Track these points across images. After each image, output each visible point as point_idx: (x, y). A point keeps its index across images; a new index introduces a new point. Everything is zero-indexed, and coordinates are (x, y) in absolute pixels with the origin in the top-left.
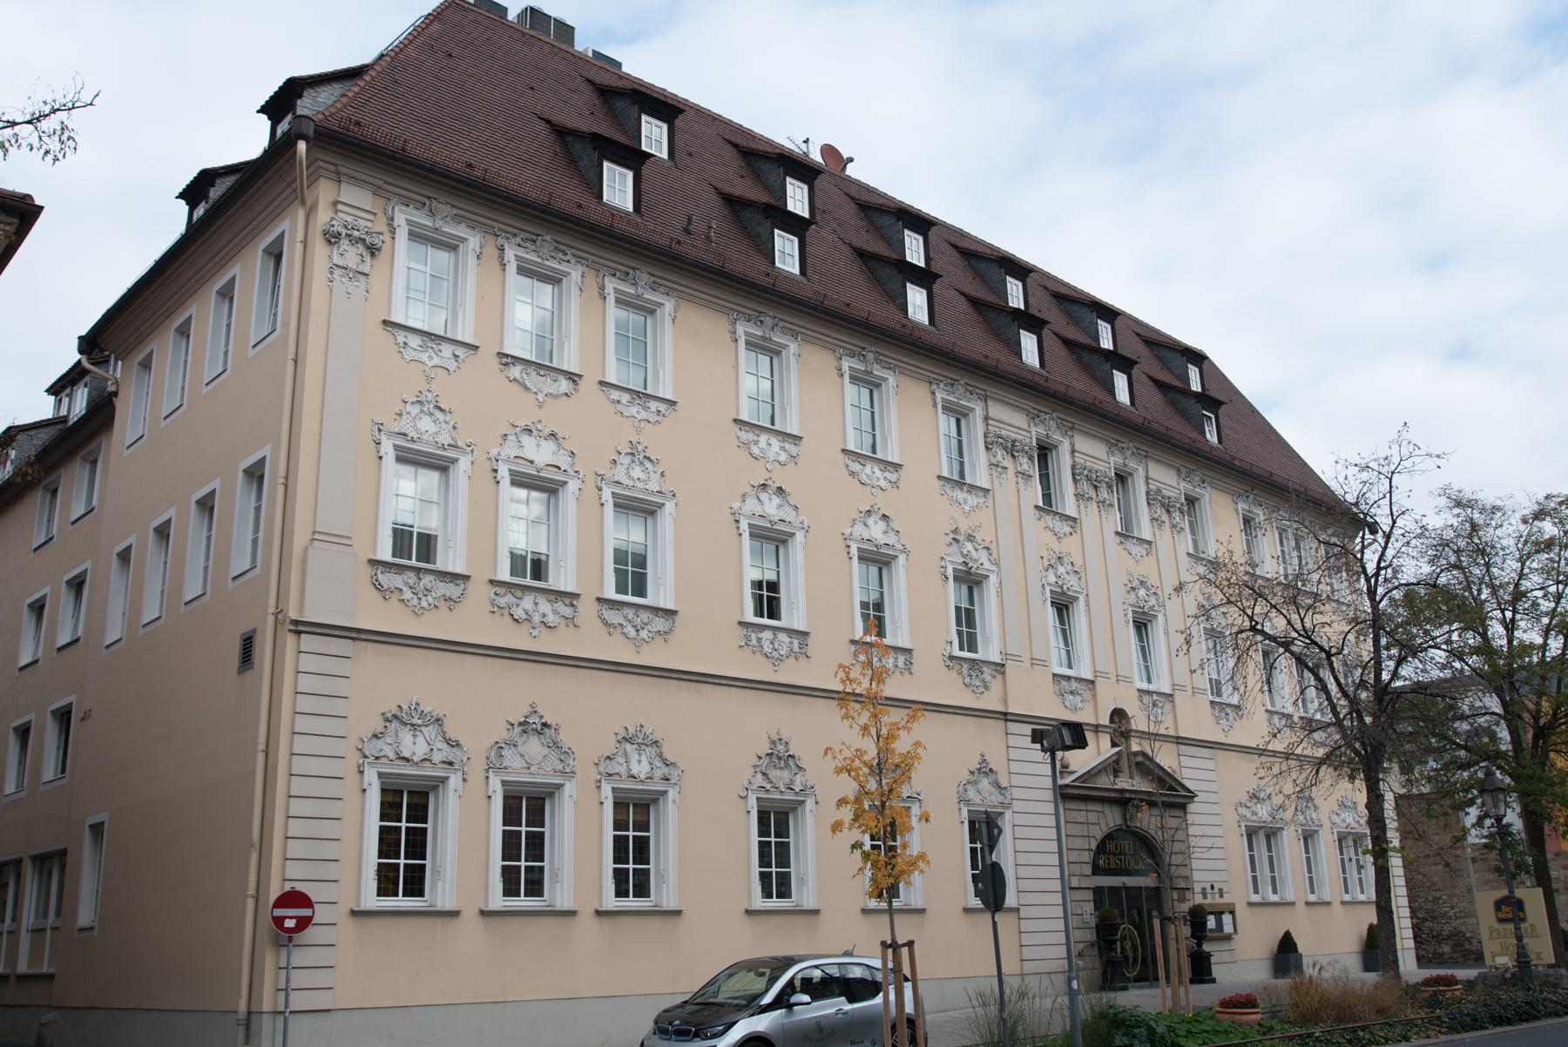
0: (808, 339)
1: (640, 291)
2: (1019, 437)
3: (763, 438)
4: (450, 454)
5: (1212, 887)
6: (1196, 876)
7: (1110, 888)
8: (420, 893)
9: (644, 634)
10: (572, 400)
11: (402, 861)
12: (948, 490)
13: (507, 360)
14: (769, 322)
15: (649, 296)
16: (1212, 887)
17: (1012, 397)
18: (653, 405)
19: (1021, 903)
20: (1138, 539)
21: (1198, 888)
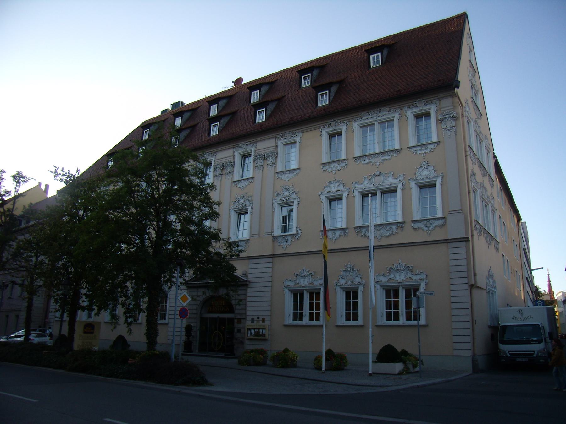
0: (349, 120)
1: (421, 109)
2: (265, 151)
3: (332, 165)
4: (338, 193)
5: (258, 318)
6: (248, 313)
7: (228, 318)
8: (398, 320)
9: (431, 228)
10: (250, 185)
11: (392, 310)
12: (280, 176)
13: (357, 158)
14: (333, 123)
15: (292, 139)
16: (258, 318)
17: (220, 148)
18: (430, 147)
19: (169, 322)
20: (289, 171)
21: (249, 318)
